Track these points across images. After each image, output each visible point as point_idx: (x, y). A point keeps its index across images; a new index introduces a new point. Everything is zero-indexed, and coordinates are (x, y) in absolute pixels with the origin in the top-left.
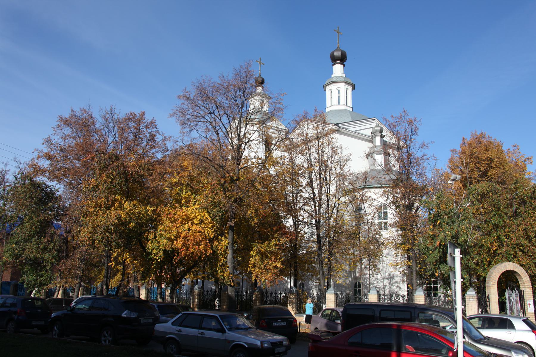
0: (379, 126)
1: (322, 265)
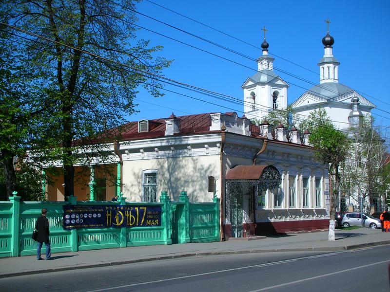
0: (356, 97)
1: (107, 65)
